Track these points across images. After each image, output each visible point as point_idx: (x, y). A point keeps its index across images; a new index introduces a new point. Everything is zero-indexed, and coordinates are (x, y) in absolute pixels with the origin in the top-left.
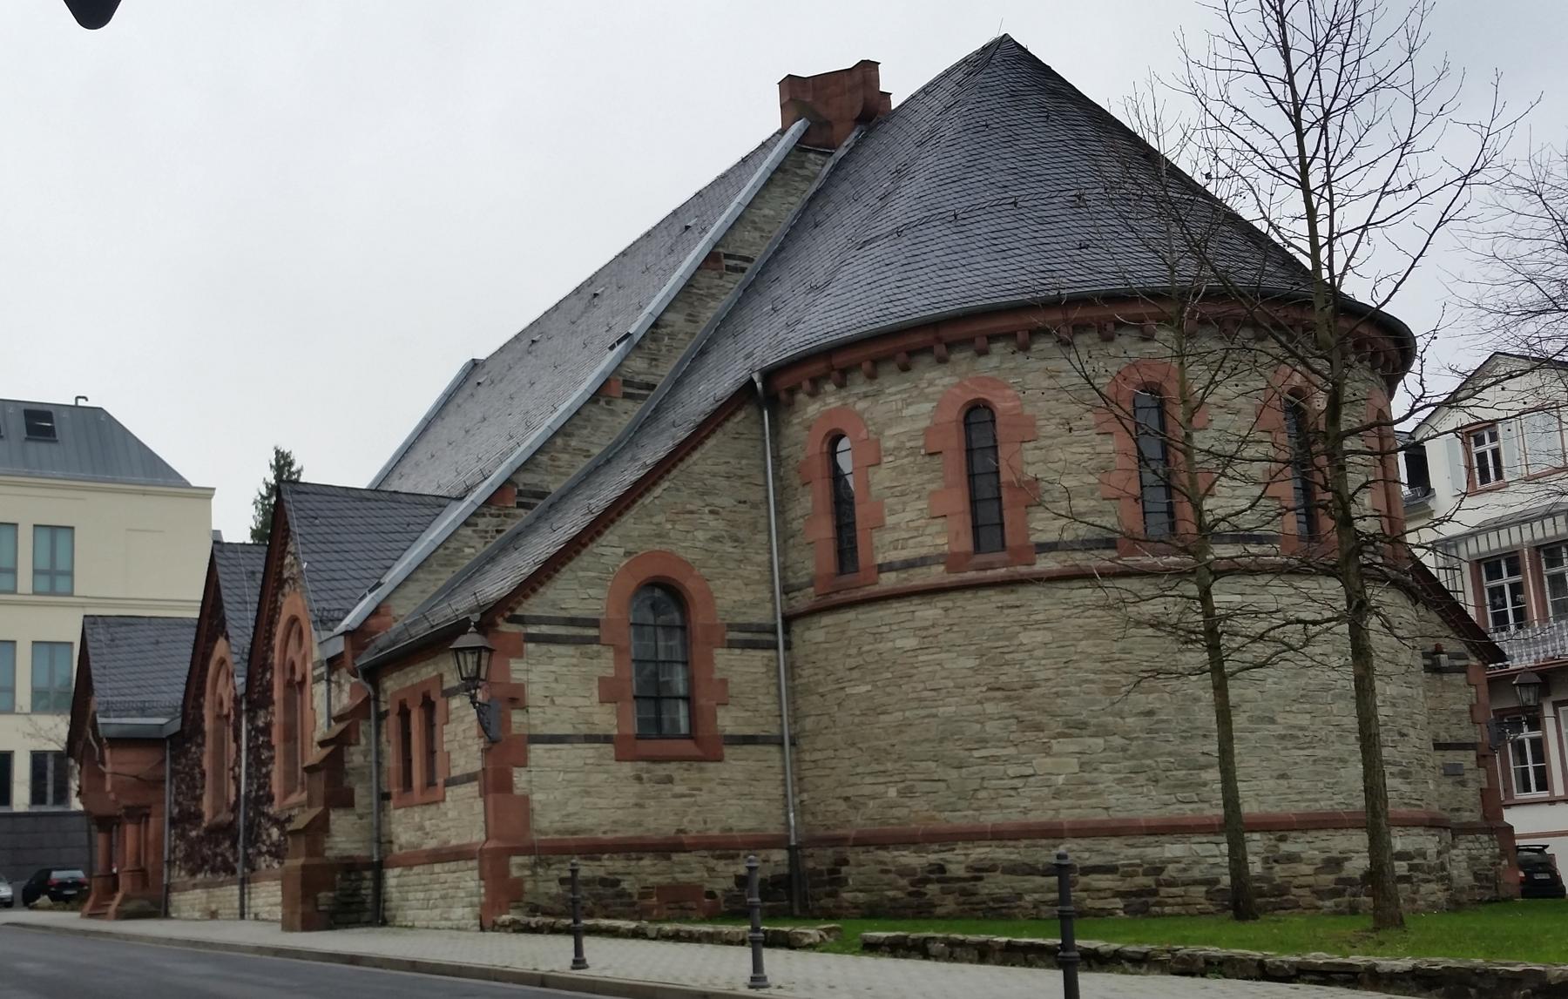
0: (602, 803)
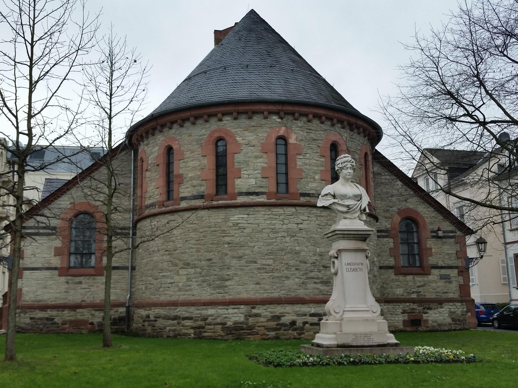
0: (51, 291)
